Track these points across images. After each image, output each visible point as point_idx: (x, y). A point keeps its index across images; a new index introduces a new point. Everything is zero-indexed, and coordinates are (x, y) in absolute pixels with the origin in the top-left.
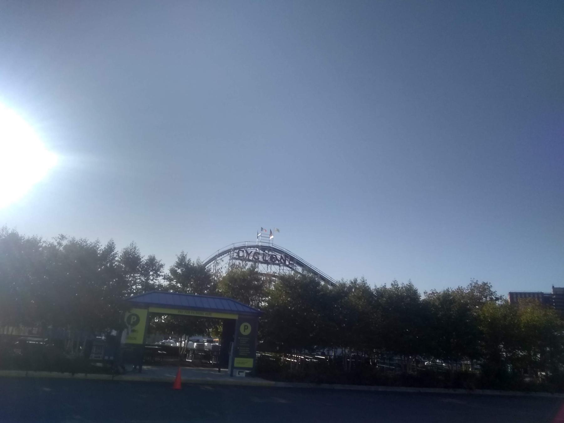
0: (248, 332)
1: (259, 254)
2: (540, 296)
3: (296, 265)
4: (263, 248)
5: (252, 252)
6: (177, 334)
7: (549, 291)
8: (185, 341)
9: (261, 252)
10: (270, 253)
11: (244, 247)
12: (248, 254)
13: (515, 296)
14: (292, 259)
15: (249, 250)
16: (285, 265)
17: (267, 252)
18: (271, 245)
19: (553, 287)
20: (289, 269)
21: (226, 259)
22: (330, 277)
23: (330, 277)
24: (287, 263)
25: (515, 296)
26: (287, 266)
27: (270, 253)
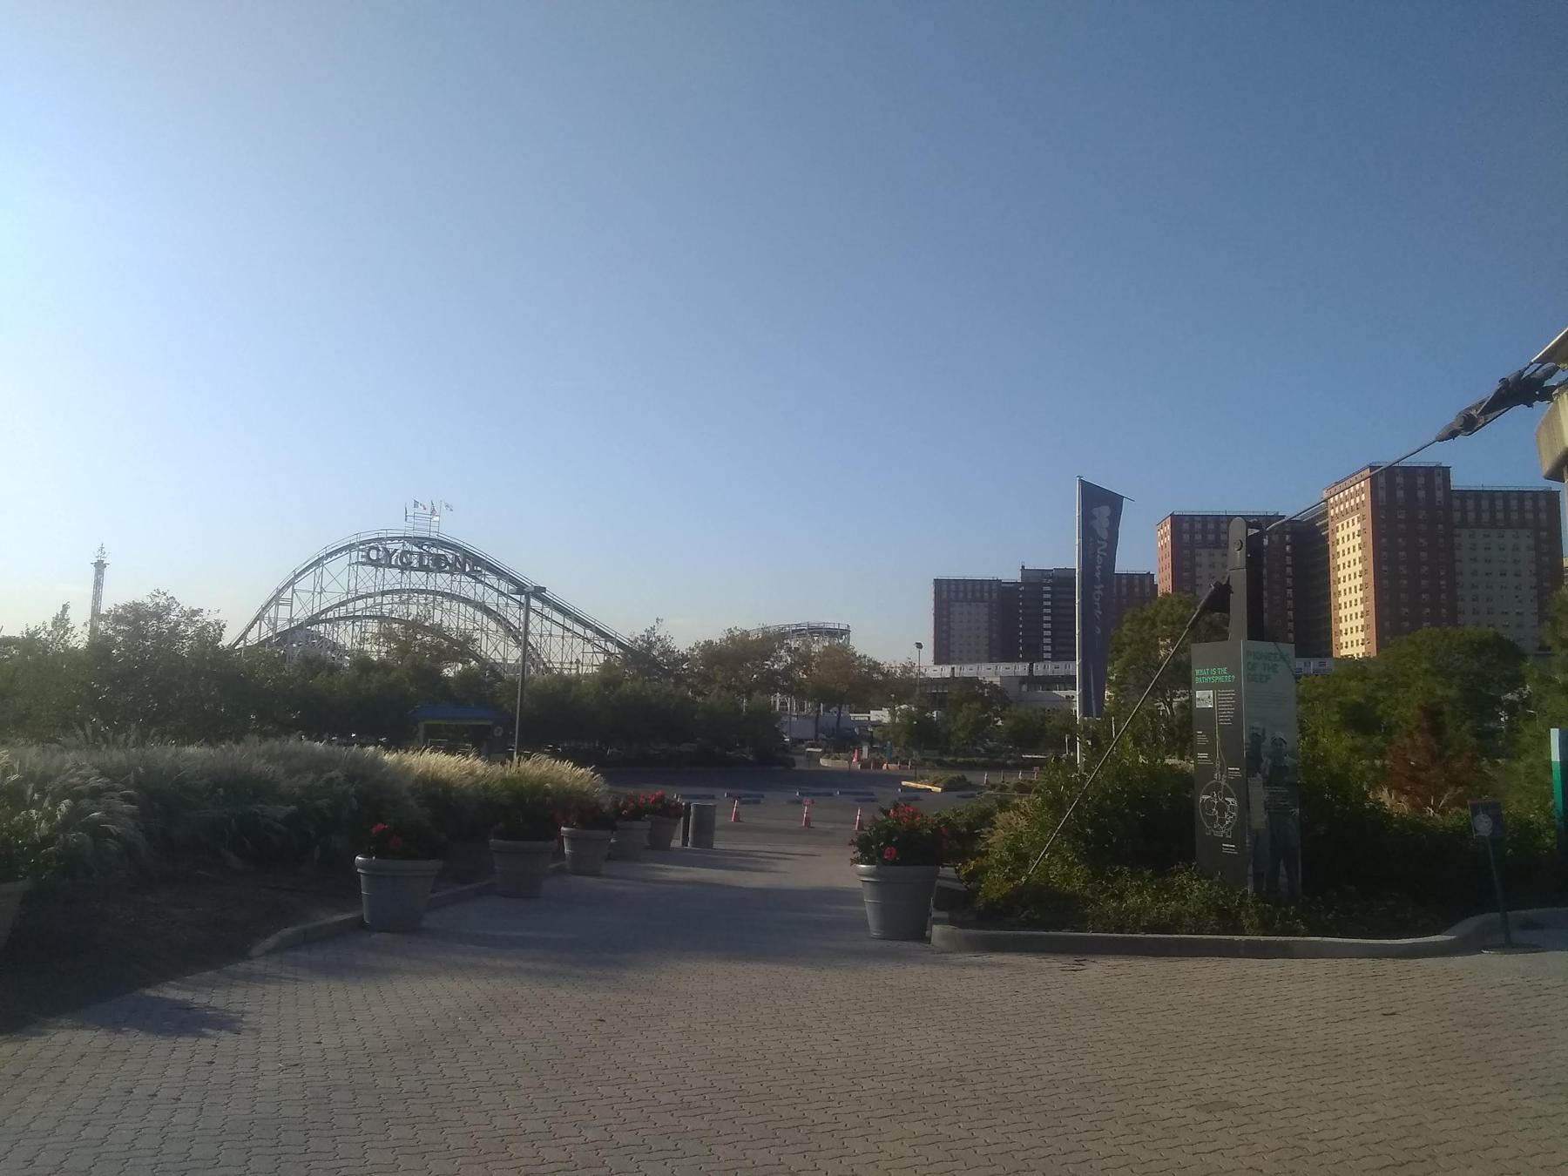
0: (500, 734)
1: (411, 553)
2: (994, 587)
3: (487, 573)
4: (419, 541)
5: (396, 550)
6: (1548, 841)
7: (1016, 577)
8: (896, 780)
9: (416, 549)
10: (434, 550)
11: (379, 540)
12: (389, 555)
13: (945, 587)
14: (477, 561)
15: (391, 547)
16: (463, 572)
17: (425, 547)
18: (434, 535)
19: (1023, 567)
20: (470, 579)
21: (339, 565)
22: (788, 859)
23: (788, 859)
24: (468, 569)
25: (945, 587)
26: (468, 574)
27: (434, 550)
